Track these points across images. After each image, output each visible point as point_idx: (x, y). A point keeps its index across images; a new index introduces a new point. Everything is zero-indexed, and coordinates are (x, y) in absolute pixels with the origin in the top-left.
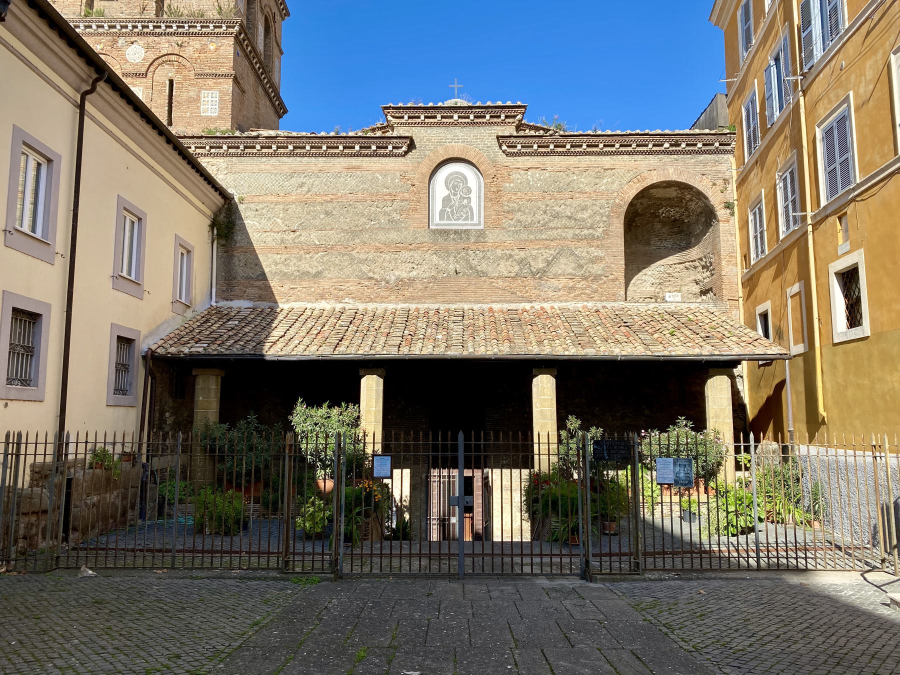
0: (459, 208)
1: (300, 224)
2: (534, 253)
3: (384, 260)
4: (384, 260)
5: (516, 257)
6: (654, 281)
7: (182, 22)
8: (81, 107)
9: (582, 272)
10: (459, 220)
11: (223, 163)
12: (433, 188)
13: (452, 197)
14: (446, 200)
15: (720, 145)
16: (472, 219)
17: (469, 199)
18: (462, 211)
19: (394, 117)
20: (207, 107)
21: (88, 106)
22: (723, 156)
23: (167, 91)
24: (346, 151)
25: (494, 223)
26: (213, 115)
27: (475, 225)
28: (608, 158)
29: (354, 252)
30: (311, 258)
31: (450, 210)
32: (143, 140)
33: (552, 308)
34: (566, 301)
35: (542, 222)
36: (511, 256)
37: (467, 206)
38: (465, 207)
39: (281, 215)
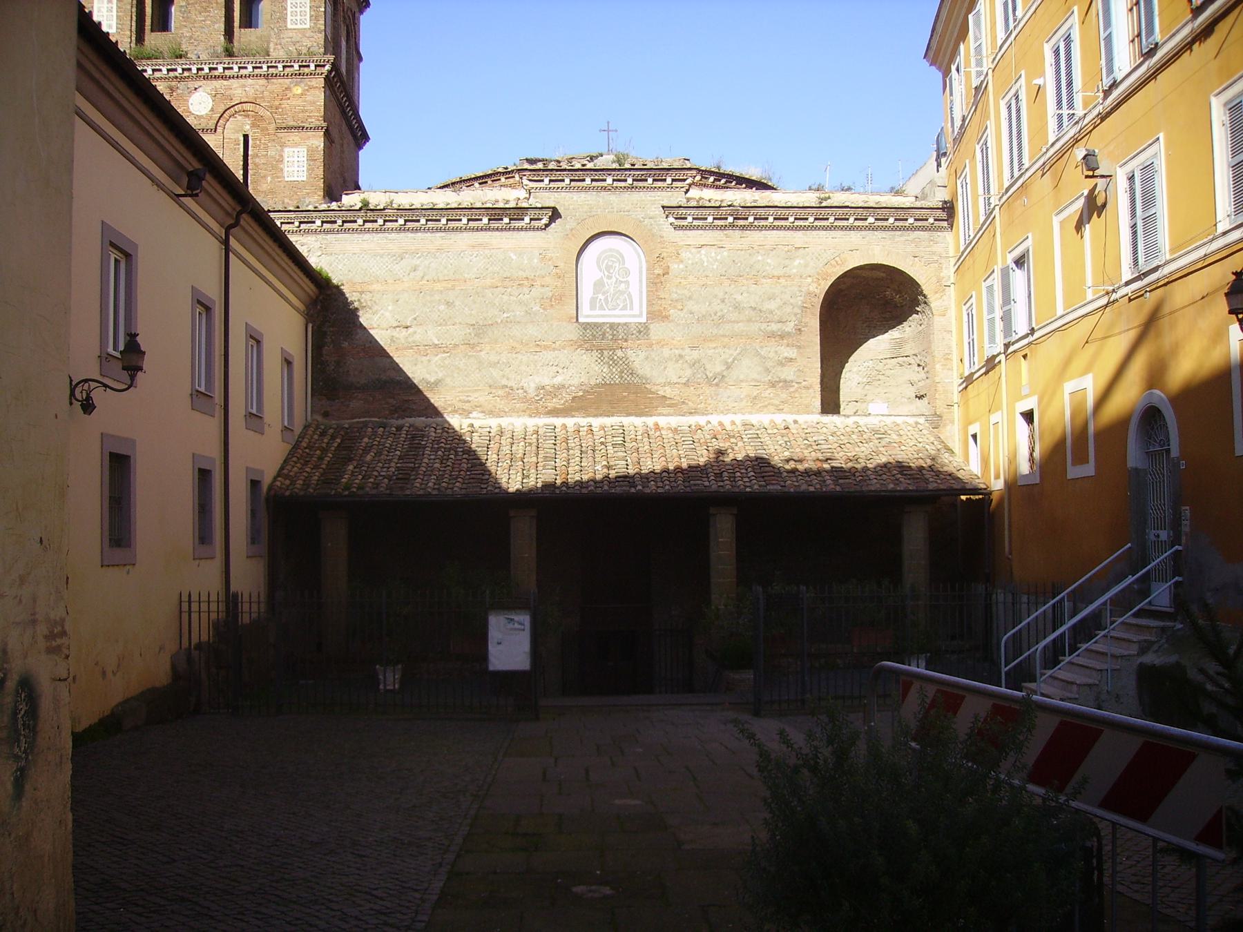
0: (614, 295)
1: (415, 319)
2: (710, 352)
3: (521, 362)
4: (521, 362)
5: (687, 358)
6: (860, 379)
7: (260, 63)
8: (226, 242)
9: (769, 378)
10: (614, 309)
11: (316, 241)
12: (581, 269)
13: (605, 280)
14: (599, 286)
15: (935, 220)
16: (632, 309)
17: (627, 283)
18: (618, 298)
19: (530, 180)
20: (293, 169)
21: (233, 242)
22: (939, 233)
23: (242, 150)
24: (472, 224)
25: (657, 314)
26: (299, 179)
27: (634, 316)
28: (800, 234)
29: (482, 353)
30: (429, 361)
31: (603, 298)
32: (261, 252)
33: (733, 423)
34: (750, 413)
35: (719, 314)
36: (681, 356)
37: (625, 292)
38: (622, 293)
39: (390, 308)
